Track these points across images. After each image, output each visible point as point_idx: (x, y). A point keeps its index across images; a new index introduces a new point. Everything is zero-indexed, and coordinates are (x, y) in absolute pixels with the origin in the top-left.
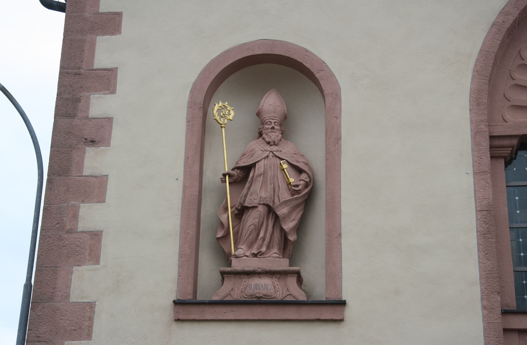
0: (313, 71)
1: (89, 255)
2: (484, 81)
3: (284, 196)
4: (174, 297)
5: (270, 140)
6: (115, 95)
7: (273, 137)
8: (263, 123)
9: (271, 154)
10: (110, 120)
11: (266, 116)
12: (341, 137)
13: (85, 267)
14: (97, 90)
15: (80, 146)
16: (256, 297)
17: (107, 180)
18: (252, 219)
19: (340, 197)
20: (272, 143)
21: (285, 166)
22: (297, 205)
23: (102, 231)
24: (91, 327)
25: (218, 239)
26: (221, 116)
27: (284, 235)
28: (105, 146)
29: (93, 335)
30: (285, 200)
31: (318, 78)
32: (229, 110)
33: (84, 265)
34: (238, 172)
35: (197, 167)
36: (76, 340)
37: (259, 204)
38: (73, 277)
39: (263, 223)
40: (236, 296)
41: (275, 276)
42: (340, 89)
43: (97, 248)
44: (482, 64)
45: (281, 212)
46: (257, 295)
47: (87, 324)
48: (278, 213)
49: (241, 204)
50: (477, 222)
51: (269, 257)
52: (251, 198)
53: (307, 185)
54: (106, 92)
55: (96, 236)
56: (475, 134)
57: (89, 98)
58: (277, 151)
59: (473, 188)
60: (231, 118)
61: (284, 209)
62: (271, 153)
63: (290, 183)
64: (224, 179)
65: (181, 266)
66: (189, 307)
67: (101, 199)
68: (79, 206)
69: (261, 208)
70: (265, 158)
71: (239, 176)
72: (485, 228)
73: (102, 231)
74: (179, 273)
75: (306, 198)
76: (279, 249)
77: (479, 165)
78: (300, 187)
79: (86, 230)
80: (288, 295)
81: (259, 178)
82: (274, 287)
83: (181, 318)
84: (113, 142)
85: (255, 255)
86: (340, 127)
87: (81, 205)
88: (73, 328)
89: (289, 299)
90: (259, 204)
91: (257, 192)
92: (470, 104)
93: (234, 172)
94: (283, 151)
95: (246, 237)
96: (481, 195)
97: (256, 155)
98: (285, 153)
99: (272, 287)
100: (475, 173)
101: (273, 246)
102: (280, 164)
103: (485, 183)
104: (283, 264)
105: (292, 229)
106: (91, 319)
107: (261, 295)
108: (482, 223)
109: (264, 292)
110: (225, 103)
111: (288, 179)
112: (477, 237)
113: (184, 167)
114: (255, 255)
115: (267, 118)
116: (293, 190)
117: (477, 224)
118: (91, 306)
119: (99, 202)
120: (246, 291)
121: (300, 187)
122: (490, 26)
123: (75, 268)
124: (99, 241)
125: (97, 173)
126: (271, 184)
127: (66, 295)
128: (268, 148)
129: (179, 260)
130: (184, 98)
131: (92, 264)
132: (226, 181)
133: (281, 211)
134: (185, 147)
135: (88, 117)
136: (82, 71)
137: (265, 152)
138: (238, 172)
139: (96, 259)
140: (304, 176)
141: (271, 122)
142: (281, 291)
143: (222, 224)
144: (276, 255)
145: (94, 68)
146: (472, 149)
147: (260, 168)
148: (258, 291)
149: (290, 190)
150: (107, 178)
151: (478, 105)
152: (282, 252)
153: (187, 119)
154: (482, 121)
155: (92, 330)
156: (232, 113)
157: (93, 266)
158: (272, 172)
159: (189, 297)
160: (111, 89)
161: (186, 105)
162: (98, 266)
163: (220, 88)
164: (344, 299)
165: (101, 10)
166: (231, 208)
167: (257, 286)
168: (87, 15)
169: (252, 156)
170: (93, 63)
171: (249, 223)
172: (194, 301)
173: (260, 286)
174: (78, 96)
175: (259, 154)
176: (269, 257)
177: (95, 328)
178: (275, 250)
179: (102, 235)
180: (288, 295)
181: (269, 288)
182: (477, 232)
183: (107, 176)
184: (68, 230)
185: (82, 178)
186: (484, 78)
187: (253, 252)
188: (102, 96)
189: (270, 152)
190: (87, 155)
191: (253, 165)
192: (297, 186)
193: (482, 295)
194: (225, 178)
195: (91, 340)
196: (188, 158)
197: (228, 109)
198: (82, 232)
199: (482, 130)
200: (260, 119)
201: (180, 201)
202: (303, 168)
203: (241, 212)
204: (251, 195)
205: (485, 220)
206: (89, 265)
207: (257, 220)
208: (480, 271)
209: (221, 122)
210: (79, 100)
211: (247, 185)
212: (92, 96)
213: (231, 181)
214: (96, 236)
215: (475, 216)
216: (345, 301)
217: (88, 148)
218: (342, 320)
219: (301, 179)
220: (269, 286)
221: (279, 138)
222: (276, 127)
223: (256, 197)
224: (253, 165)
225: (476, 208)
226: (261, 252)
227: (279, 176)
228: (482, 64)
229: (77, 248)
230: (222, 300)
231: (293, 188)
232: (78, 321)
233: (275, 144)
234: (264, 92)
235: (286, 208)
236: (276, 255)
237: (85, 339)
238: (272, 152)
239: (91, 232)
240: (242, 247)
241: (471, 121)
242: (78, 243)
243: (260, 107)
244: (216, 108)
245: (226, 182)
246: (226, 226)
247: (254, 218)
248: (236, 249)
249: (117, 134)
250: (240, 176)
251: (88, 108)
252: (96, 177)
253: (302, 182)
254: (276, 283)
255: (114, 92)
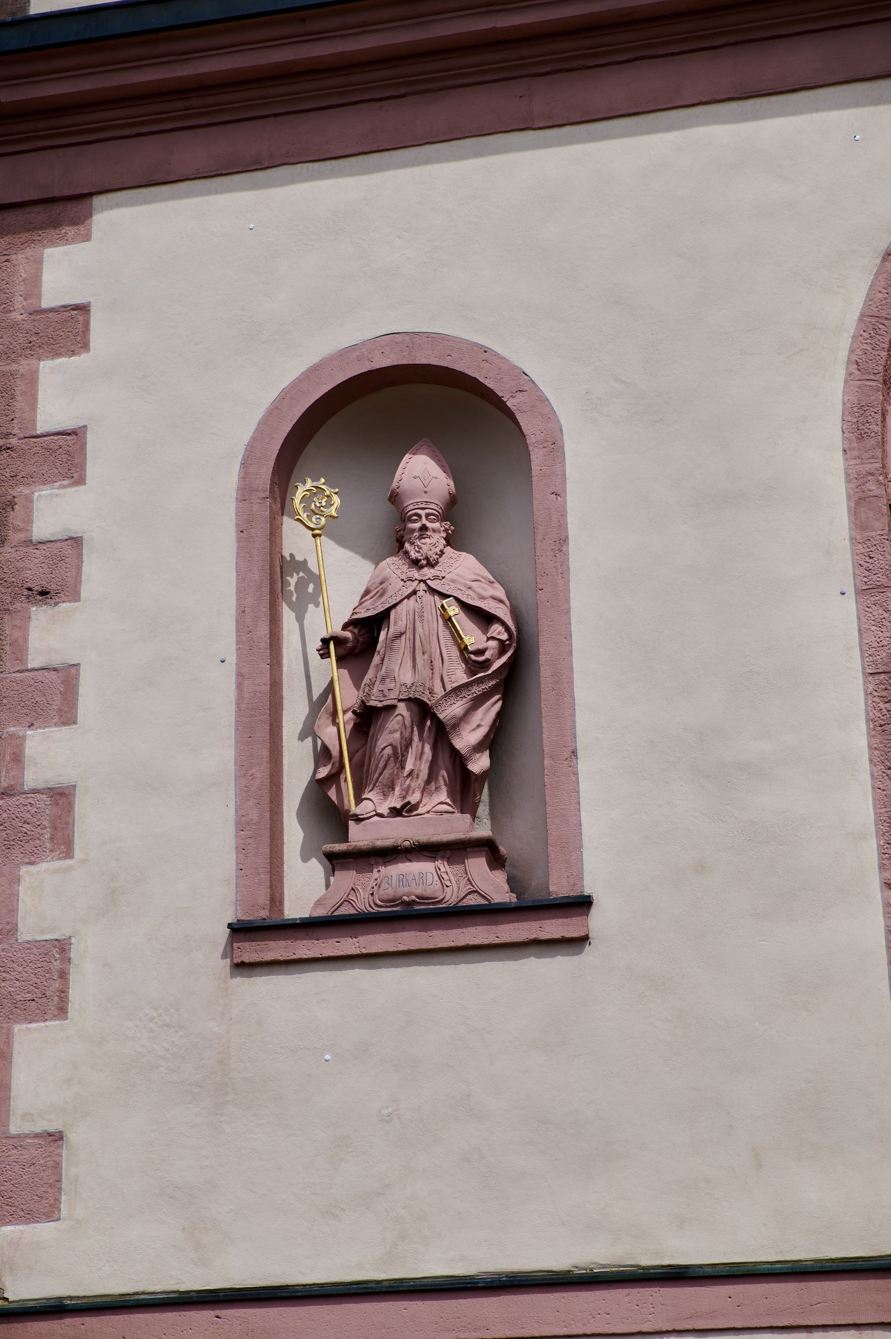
0: (500, 394)
1: (51, 839)
2: (871, 383)
3: (453, 677)
4: (230, 917)
5: (418, 556)
6: (84, 487)
7: (425, 548)
8: (405, 518)
9: (422, 586)
10: (76, 542)
11: (410, 504)
12: (567, 537)
13: (44, 866)
14: (46, 481)
15: (18, 605)
16: (404, 903)
17: (78, 674)
18: (389, 735)
19: (571, 669)
20: (424, 562)
21: (453, 610)
22: (484, 694)
23: (75, 786)
24: (63, 993)
25: (321, 782)
26: (312, 511)
27: (458, 760)
28: (70, 601)
29: (69, 1010)
30: (455, 685)
31: (513, 408)
32: (328, 496)
33: (42, 861)
34: (356, 631)
35: (263, 630)
36: (37, 1021)
37: (400, 700)
38: (20, 888)
39: (411, 739)
40: (363, 903)
41: (441, 853)
42: (561, 430)
43: (67, 823)
44: (866, 346)
45: (447, 712)
46: (405, 898)
47: (57, 985)
48: (441, 716)
49: (363, 701)
50: (866, 700)
51: (428, 812)
52: (381, 687)
53: (503, 648)
54: (65, 483)
55: (62, 796)
56: (857, 504)
57: (29, 499)
58: (436, 578)
59: (856, 626)
60: (333, 511)
61: (454, 706)
62: (422, 584)
63: (466, 647)
64: (326, 651)
65: (241, 849)
66: (261, 938)
67: (67, 716)
68: (24, 737)
69: (402, 708)
70: (408, 597)
71: (358, 641)
72: (884, 711)
73: (75, 786)
74: (237, 864)
75: (503, 677)
76: (451, 794)
77: (867, 573)
78: (488, 655)
79: (41, 785)
80: (469, 893)
81: (398, 641)
82: (440, 878)
83: (247, 961)
84: (85, 591)
85: (396, 812)
86: (563, 515)
87: (29, 733)
88: (29, 996)
89: (473, 901)
90: (400, 700)
91: (398, 672)
92: (845, 439)
93: (348, 634)
94: (447, 576)
95: (376, 775)
96: (873, 639)
97: (389, 594)
98: (453, 581)
99: (436, 878)
100: (860, 592)
101: (437, 789)
102: (442, 606)
103: (881, 611)
104: (459, 827)
105: (478, 748)
106: (63, 975)
107: (414, 898)
108: (878, 700)
109: (419, 891)
110: (319, 480)
111: (461, 638)
112: (868, 733)
113: (237, 631)
114: (396, 812)
115: (411, 507)
116: (474, 663)
117: (866, 705)
118: (63, 947)
119: (64, 724)
120: (381, 892)
121: (488, 655)
122: (879, 260)
123: (24, 870)
124: (69, 808)
125: (56, 660)
126: (423, 653)
127: (8, 927)
128: (415, 574)
129: (237, 836)
130: (230, 479)
131: (59, 859)
132: (329, 653)
133: (450, 711)
134: (238, 589)
135: (31, 541)
136: (14, 441)
137: (409, 583)
138: (356, 631)
139: (63, 844)
140: (497, 630)
141: (420, 516)
142: (455, 885)
143: (326, 750)
144: (445, 807)
145: (38, 432)
146: (851, 539)
147: (399, 620)
148: (407, 889)
149: (466, 661)
150: (78, 671)
151: (861, 438)
152: (458, 797)
153: (237, 525)
154: (872, 474)
155: (67, 997)
156: (336, 500)
157: (61, 862)
158: (426, 629)
159: (262, 914)
160: (76, 475)
161: (234, 495)
162: (69, 862)
163: (310, 449)
164: (587, 891)
165: (46, 303)
166: (345, 712)
167: (402, 878)
168: (16, 316)
169: (382, 595)
170: (34, 422)
171: (382, 742)
172: (275, 919)
173: (410, 878)
174: (10, 497)
175: (396, 589)
176: (428, 812)
177: (74, 994)
178: (443, 796)
179: (74, 795)
180: (469, 893)
181: (430, 881)
182: (869, 720)
183: (77, 665)
184: (5, 789)
185: (28, 674)
186: (872, 377)
187: (392, 805)
188: (57, 491)
189: (420, 581)
190: (33, 624)
191: (383, 618)
192: (481, 652)
193: (881, 859)
194: (328, 648)
195: (66, 1018)
196: (244, 612)
197: (328, 493)
198: (35, 791)
199: (871, 494)
200: (397, 507)
201: (233, 707)
202: (492, 611)
203: (368, 718)
204: (383, 680)
205: (884, 694)
206: (52, 860)
207: (397, 735)
208: (875, 806)
209: (312, 525)
210: (11, 504)
211: (376, 659)
212: (36, 494)
213: (342, 651)
214: (62, 796)
215: (862, 688)
216: (589, 897)
217: (34, 609)
218: (582, 941)
219: (489, 635)
220: (429, 875)
221: (438, 550)
222: (429, 525)
223: (392, 685)
224: (383, 618)
225: (864, 668)
226: (409, 803)
227: (441, 634)
228: (866, 346)
229: (26, 826)
230: (331, 916)
231: (473, 657)
232: (38, 981)
233: (431, 564)
234: (407, 446)
235: (459, 703)
236: (445, 807)
237: (55, 1017)
238: (424, 582)
239: (52, 789)
240: (370, 795)
241: (847, 475)
242: (28, 815)
243: (394, 485)
244: (300, 493)
245: (329, 657)
246: (335, 752)
247: (391, 732)
248: (359, 800)
249: (94, 574)
250: (361, 639)
251: (28, 520)
252: (55, 670)
253: (493, 644)
254: (443, 869)
255: (81, 481)
